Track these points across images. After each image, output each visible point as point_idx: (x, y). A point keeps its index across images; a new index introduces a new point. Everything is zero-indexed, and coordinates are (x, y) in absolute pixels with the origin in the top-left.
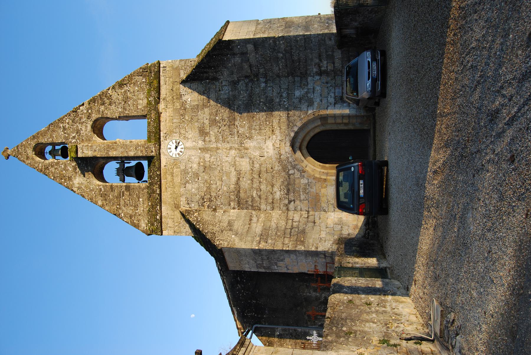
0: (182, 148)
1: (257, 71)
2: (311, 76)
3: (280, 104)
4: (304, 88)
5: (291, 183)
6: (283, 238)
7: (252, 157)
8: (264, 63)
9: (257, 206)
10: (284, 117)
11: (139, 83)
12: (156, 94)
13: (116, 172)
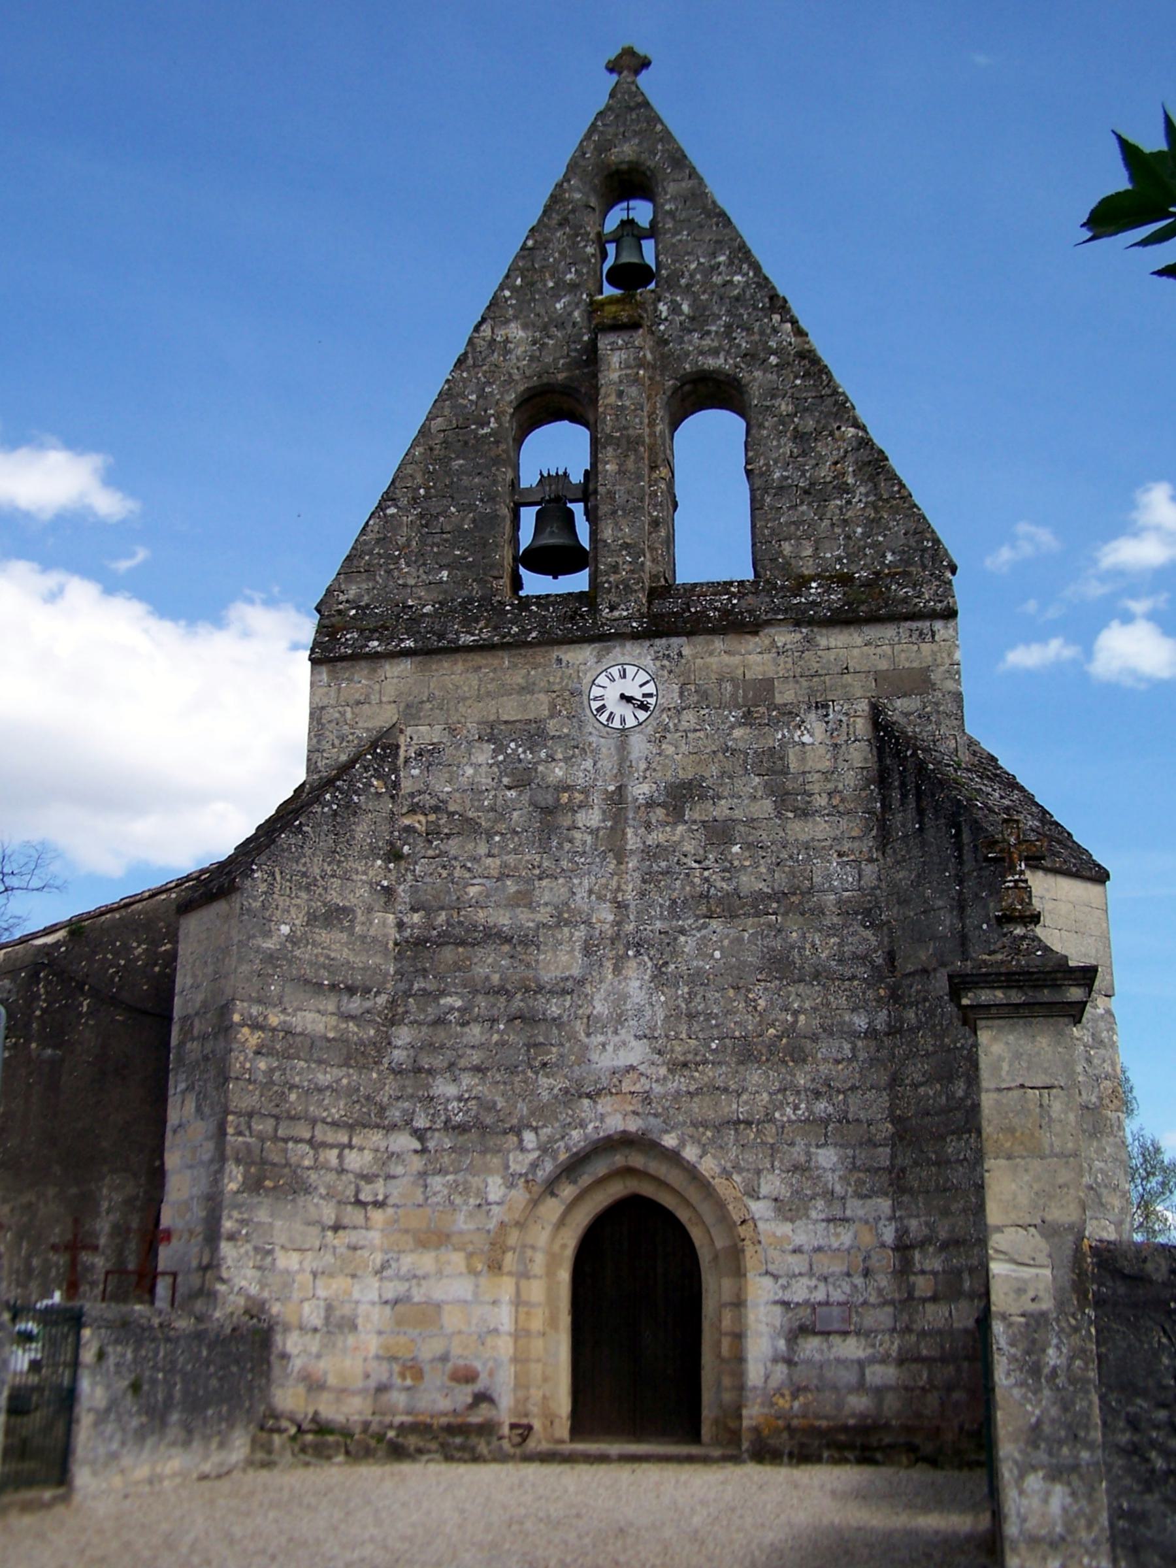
0: (623, 721)
1: (910, 996)
2: (894, 1211)
3: (785, 1089)
4: (849, 1184)
5: (488, 1136)
6: (276, 1111)
7: (588, 989)
8: (934, 1026)
9: (407, 1012)
10: (735, 1106)
11: (881, 539)
12: (829, 609)
13: (553, 473)
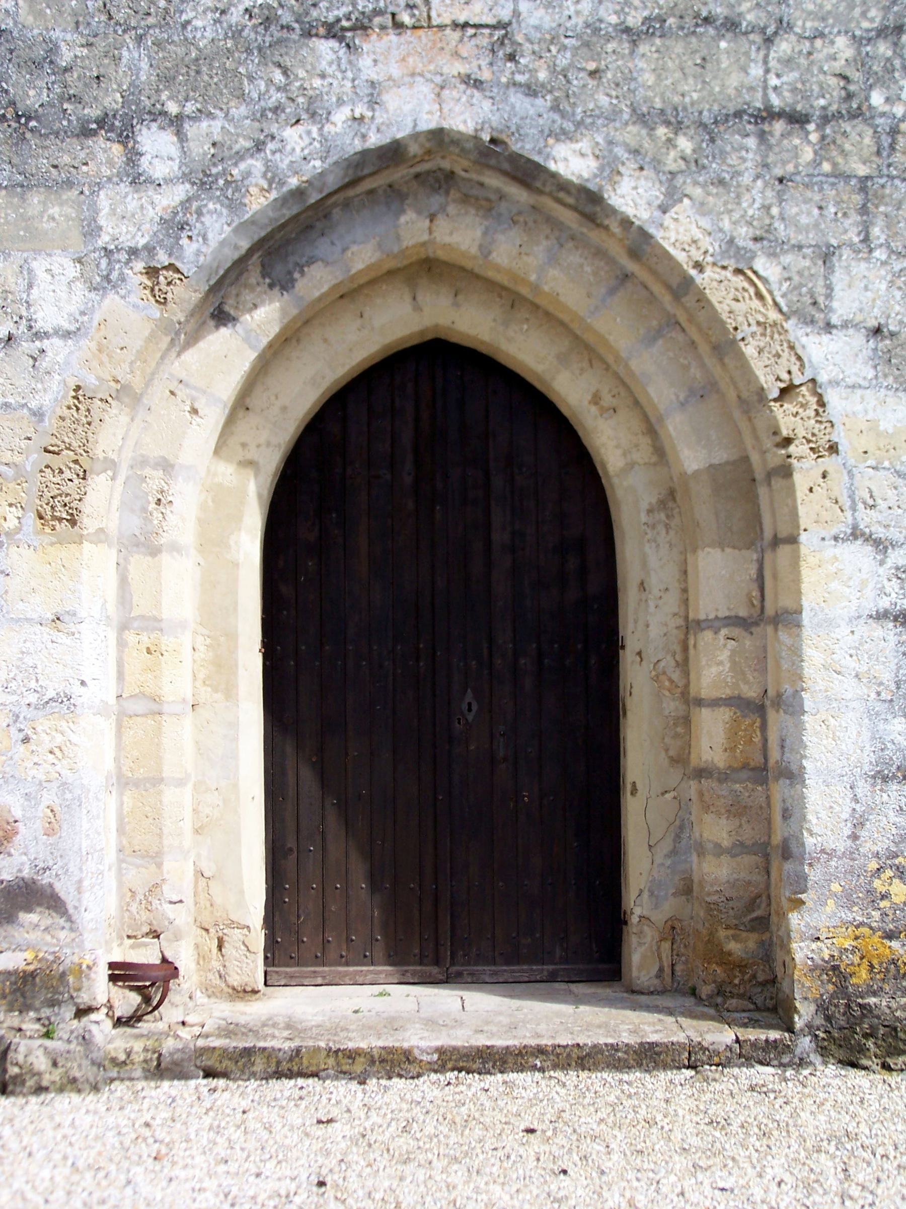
10: (756, 71)
